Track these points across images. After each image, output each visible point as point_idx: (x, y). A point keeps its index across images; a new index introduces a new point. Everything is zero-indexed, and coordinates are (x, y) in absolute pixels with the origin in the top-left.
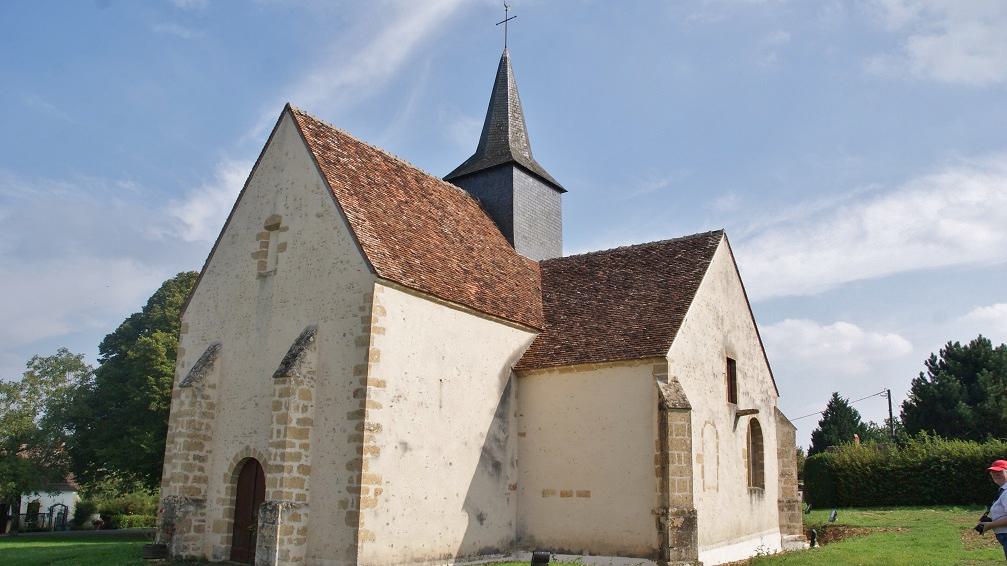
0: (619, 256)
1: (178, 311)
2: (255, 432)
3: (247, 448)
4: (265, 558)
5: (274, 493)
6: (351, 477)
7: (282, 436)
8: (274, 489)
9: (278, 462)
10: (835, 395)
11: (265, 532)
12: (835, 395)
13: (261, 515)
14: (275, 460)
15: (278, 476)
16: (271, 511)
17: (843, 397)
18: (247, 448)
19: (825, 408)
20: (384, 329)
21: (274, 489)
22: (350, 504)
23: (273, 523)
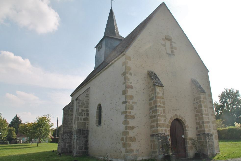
0: (195, 82)
1: (34, 142)
2: (178, 109)
3: (176, 115)
4: (211, 152)
5: (208, 130)
6: (214, 126)
7: (207, 111)
8: (208, 129)
9: (207, 120)
10: (17, 115)
11: (210, 143)
12: (17, 115)
13: (207, 138)
14: (206, 119)
15: (208, 125)
16: (210, 136)
17: (18, 116)
18: (176, 115)
19: (13, 118)
20: (136, 103)
21: (208, 129)
22: (215, 133)
23: (212, 140)
